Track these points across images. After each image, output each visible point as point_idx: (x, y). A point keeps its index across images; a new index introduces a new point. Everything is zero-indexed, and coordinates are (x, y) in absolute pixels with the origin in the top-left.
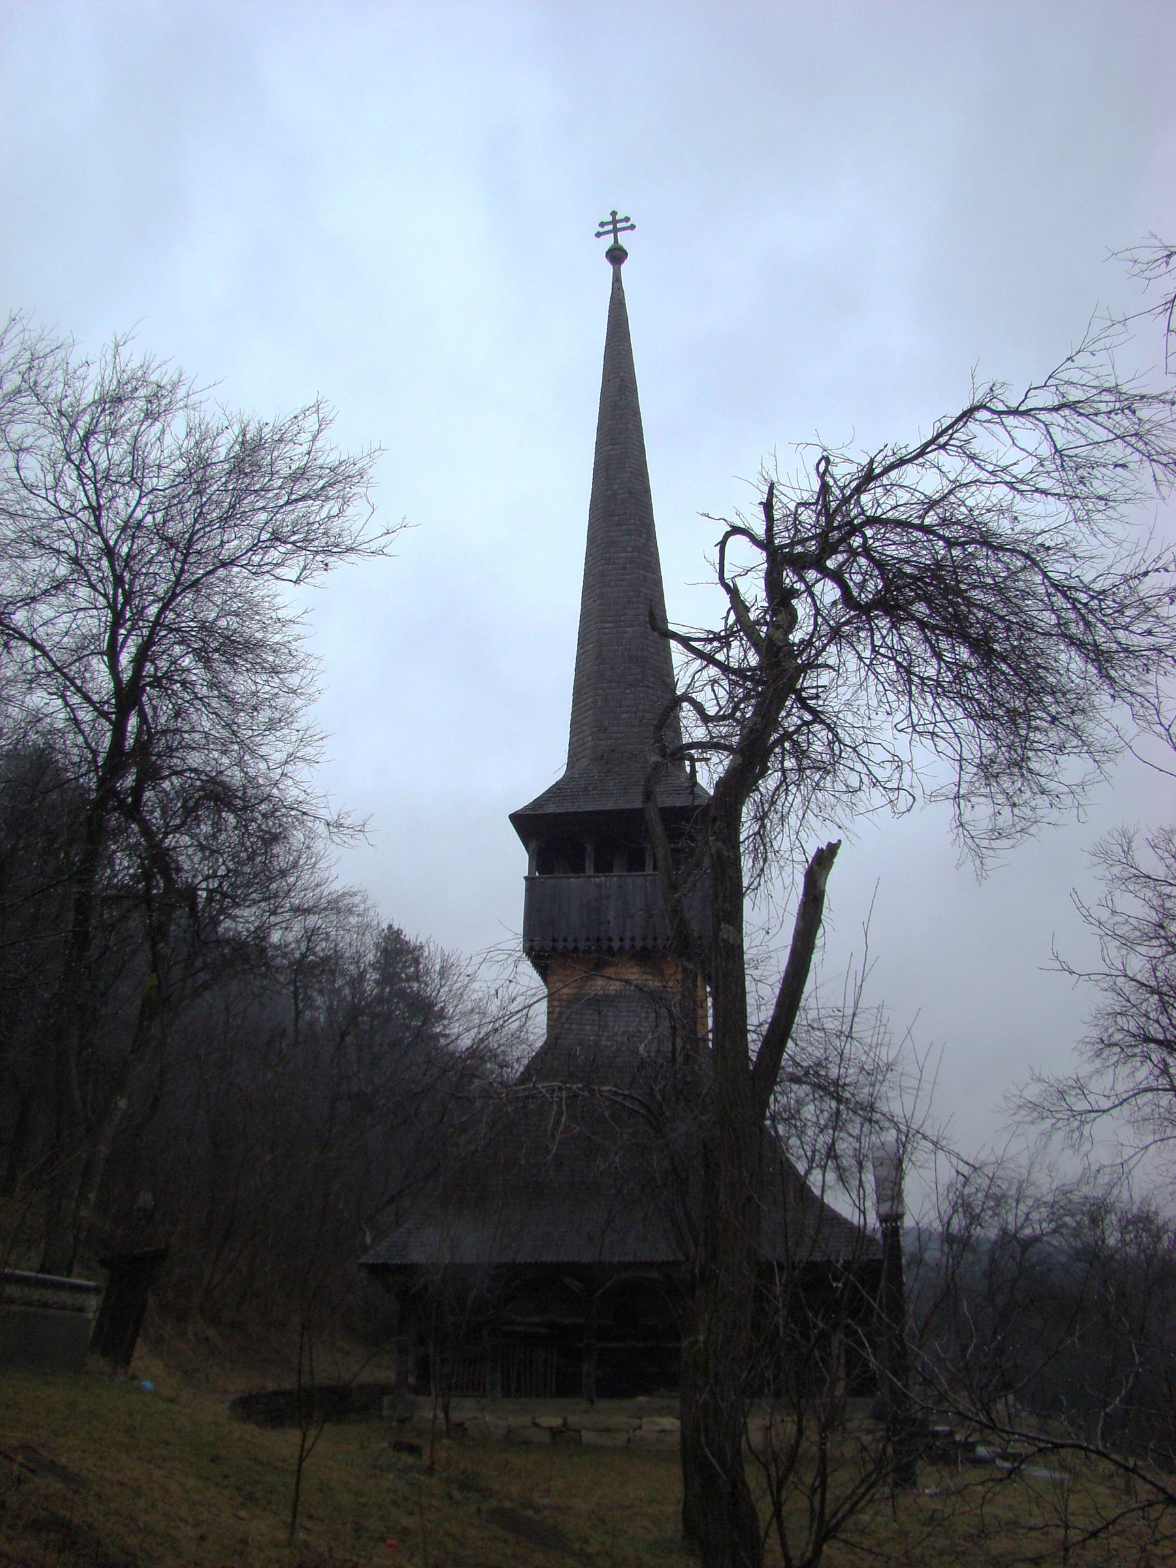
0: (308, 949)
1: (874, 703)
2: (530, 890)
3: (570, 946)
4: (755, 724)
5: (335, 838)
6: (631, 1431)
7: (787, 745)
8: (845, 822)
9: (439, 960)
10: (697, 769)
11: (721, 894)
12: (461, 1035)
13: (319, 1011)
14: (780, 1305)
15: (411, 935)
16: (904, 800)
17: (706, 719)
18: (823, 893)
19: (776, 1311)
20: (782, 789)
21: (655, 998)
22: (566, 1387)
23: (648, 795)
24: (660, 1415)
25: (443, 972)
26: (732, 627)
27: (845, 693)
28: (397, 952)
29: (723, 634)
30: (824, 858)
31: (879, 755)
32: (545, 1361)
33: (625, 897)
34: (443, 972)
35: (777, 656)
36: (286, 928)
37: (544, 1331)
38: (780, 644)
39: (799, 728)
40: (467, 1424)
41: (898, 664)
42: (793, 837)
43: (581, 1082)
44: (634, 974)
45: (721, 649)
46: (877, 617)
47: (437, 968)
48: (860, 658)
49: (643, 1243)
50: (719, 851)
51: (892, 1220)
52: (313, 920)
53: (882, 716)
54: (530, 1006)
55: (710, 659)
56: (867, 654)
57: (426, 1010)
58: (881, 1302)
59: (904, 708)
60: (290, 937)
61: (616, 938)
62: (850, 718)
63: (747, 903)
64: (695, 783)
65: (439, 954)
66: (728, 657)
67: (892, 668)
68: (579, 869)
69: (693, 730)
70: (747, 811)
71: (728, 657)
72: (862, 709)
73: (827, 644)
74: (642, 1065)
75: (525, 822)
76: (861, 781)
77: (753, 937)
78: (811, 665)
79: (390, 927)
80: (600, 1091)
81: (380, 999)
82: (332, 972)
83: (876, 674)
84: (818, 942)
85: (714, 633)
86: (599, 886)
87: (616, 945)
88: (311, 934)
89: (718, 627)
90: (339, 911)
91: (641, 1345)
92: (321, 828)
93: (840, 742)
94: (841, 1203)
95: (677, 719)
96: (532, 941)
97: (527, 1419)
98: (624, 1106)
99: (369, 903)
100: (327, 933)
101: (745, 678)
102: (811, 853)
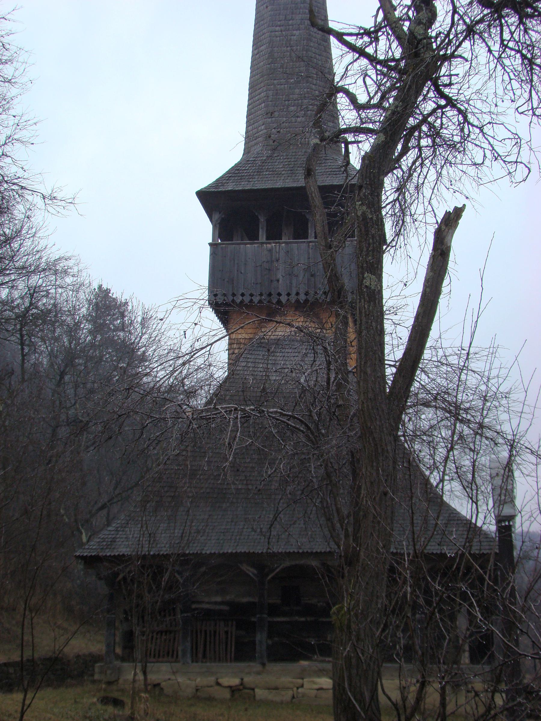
0: (31, 304)
1: (500, 92)
2: (213, 255)
3: (247, 299)
4: (397, 107)
5: (50, 209)
6: (295, 689)
7: (424, 128)
8: (472, 194)
9: (140, 313)
10: (350, 150)
11: (365, 249)
12: (159, 374)
13: (42, 356)
14: (408, 576)
15: (118, 293)
16: (521, 171)
17: (358, 107)
18: (448, 249)
19: (405, 582)
20: (417, 164)
21: (314, 340)
22: (243, 653)
23: (309, 173)
24: (319, 676)
25: (144, 322)
26: (380, 24)
27: (476, 82)
28: (106, 307)
29: (372, 29)
30: (451, 219)
31: (501, 132)
32: (227, 632)
33: (291, 260)
34: (144, 322)
35: (417, 47)
36: (12, 287)
37: (225, 608)
38: (419, 37)
39: (434, 111)
40: (163, 684)
41: (523, 57)
42: (426, 204)
43: (253, 404)
44: (299, 321)
45: (371, 43)
46: (507, 15)
47: (139, 319)
48: (490, 51)
49: (302, 537)
50: (364, 213)
51: (505, 525)
52: (35, 280)
53: (507, 103)
54: (212, 344)
55: (362, 53)
56: (496, 48)
57: (130, 355)
58: (490, 575)
59: (526, 95)
60: (16, 294)
61: (284, 293)
62: (479, 104)
63: (386, 258)
64: (348, 163)
65: (140, 308)
66: (376, 51)
67: (518, 60)
68: (253, 237)
69: (348, 116)
70: (389, 183)
71: (376, 51)
72: (490, 98)
73: (463, 40)
74: (304, 391)
75: (209, 198)
76: (485, 156)
77: (394, 288)
78: (447, 58)
79: (100, 287)
80: (268, 411)
81: (92, 345)
82: (53, 323)
83: (503, 67)
84: (445, 289)
85: (365, 30)
86: (270, 251)
87: (284, 299)
88: (33, 292)
89: (369, 24)
90: (56, 273)
91: (303, 619)
92: (38, 200)
93: (469, 123)
94: (462, 506)
95: (335, 104)
96: (216, 295)
97: (211, 680)
98: (288, 424)
99: (81, 266)
100: (47, 291)
101: (390, 68)
102: (440, 216)
